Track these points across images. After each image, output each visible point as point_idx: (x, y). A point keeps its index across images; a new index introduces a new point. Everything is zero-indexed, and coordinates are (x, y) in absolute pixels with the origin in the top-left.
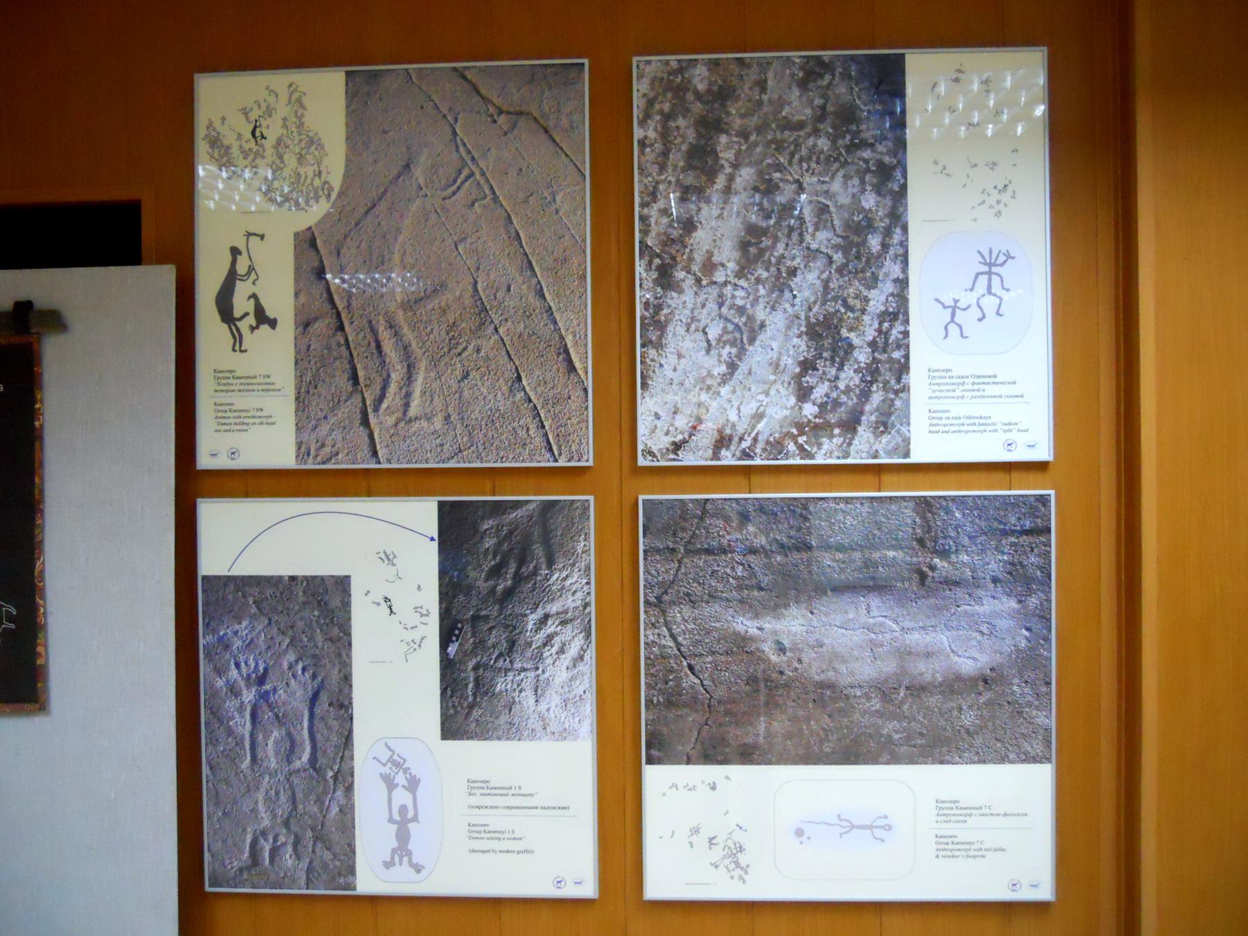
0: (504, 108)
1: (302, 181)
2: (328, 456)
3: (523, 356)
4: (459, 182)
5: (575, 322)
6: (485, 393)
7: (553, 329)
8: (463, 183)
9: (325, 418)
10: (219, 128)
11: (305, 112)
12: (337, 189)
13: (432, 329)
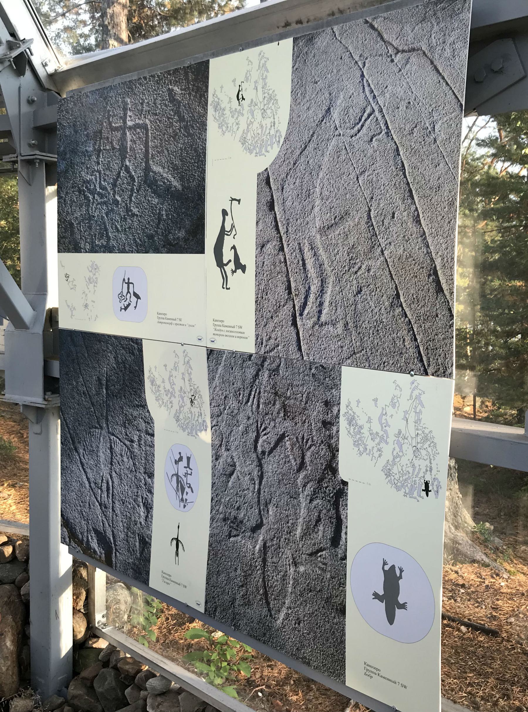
0: (400, 48)
1: (416, 473)
2: (273, 347)
3: (401, 276)
4: (363, 120)
5: (444, 246)
6: (373, 307)
7: (425, 252)
8: (366, 120)
9: (272, 317)
10: (355, 409)
11: (268, 74)
12: (284, 135)
13: (338, 251)
